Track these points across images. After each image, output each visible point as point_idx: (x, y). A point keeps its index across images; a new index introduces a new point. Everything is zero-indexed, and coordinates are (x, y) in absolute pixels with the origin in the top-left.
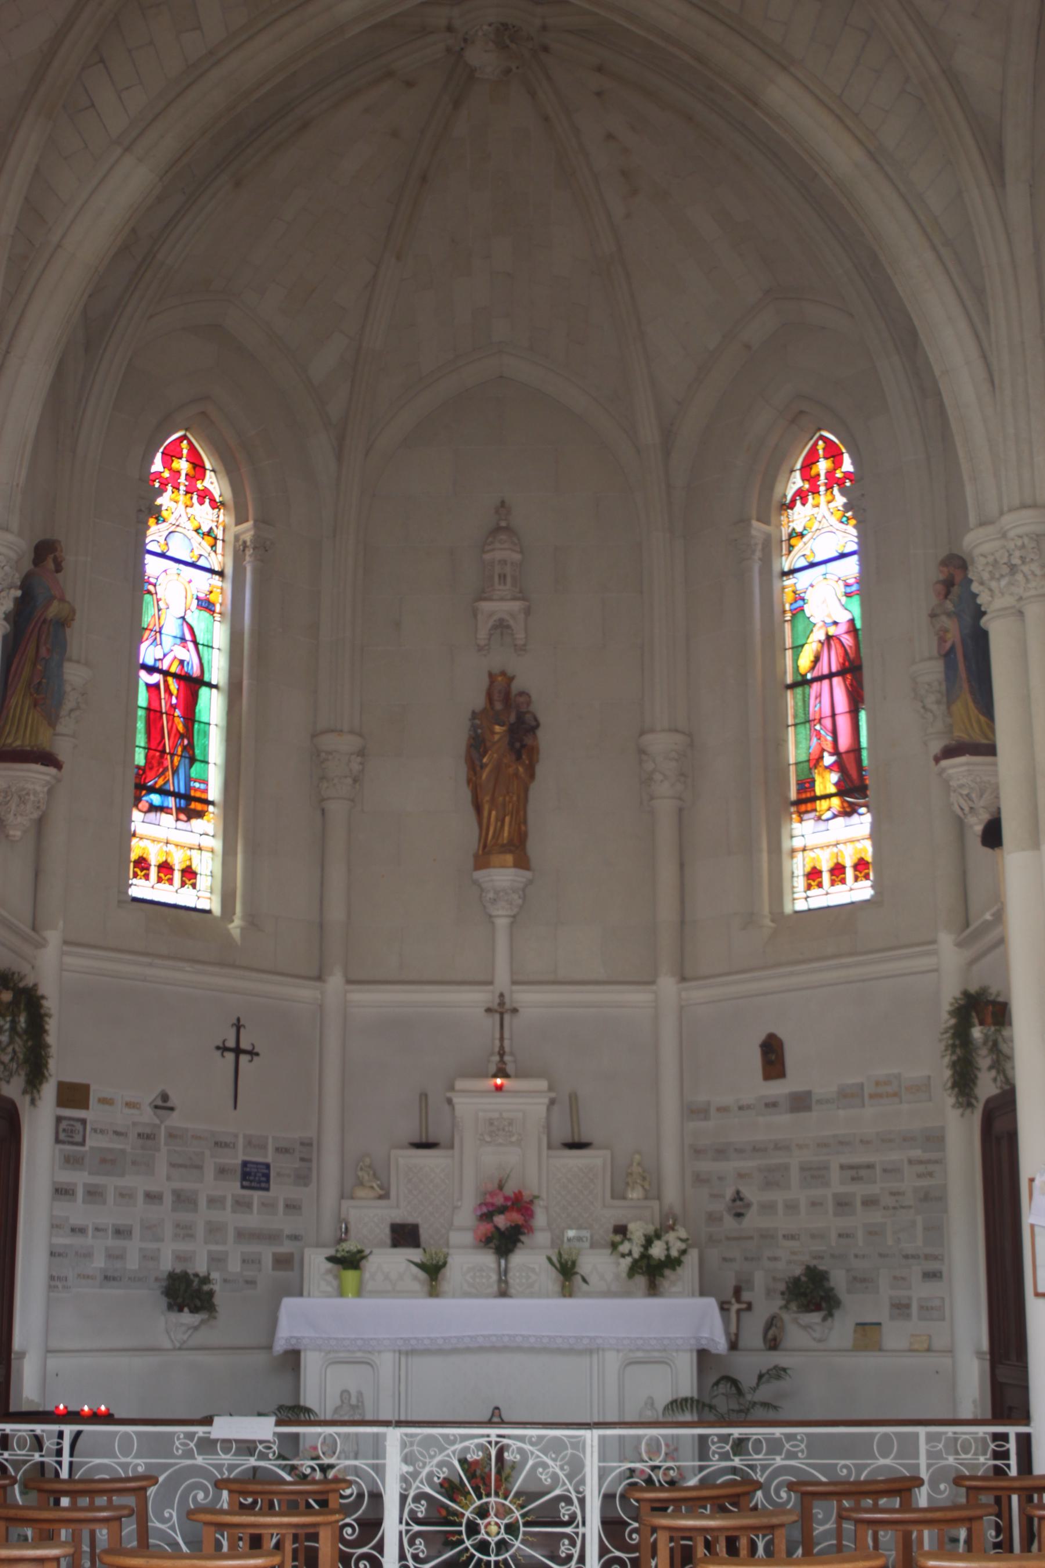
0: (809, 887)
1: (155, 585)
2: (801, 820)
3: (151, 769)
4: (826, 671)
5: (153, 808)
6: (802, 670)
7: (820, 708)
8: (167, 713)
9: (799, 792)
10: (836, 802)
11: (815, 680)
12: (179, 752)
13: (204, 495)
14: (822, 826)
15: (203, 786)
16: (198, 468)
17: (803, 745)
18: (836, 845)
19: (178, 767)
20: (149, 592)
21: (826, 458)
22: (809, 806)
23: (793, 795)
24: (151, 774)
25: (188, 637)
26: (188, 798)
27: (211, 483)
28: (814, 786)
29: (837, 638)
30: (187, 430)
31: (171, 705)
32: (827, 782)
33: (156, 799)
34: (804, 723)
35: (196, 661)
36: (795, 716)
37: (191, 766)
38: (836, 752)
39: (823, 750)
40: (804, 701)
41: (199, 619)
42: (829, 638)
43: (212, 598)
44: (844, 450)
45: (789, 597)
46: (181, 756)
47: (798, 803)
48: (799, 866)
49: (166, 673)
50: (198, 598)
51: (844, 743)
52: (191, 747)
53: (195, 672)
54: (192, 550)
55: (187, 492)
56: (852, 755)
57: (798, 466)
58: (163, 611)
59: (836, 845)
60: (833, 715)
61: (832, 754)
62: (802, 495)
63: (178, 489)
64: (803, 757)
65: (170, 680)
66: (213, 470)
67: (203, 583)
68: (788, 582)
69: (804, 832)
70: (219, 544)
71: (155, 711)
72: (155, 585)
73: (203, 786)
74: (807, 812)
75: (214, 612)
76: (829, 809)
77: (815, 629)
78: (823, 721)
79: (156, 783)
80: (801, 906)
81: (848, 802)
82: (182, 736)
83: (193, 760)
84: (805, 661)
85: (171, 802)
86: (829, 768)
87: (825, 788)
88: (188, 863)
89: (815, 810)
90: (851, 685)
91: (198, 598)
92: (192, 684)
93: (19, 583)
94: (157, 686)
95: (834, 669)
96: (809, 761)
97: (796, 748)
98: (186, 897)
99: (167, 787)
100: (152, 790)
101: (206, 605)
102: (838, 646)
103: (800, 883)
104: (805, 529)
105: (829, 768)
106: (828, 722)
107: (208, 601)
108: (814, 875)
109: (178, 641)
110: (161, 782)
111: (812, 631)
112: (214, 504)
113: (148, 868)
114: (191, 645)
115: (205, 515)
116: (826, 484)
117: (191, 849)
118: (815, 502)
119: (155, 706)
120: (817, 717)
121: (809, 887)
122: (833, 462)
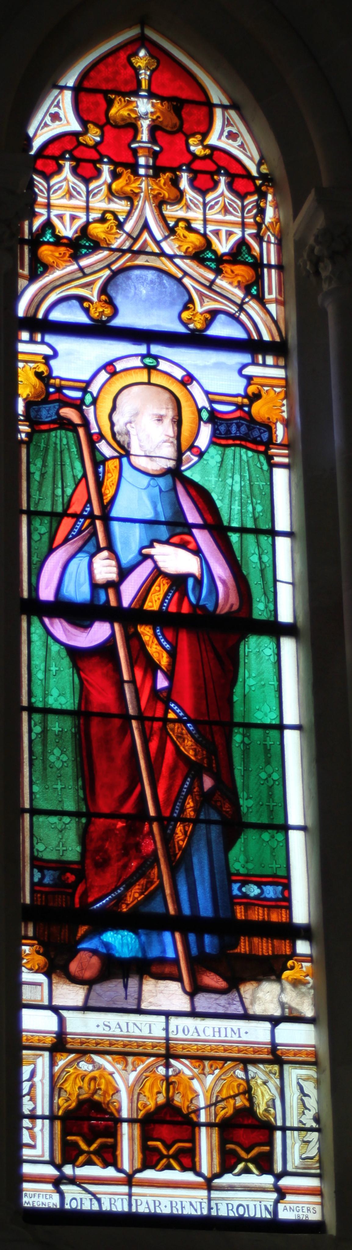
0: (69, 1154)
1: (78, 405)
3: (102, 865)
5: (114, 968)
8: (140, 718)
12: (190, 813)
13: (212, 169)
15: (270, 892)
16: (186, 111)
19: (187, 852)
20: (66, 424)
21: (151, 95)
24: (109, 876)
25: (193, 517)
26: (226, 927)
27: (229, 136)
30: (143, 24)
31: (155, 693)
33: (121, 942)
35: (220, 570)
37: (229, 844)
41: (218, 472)
43: (259, 410)
46: (195, 821)
49: (131, 617)
50: (214, 418)
52: (227, 789)
53: (225, 596)
54: (188, 304)
55: (157, 171)
57: (70, 80)
58: (112, 465)
63: (134, 167)
65: (146, 632)
66: (234, 106)
67: (219, 376)
70: (271, 278)
71: (105, 716)
72: (78, 405)
73: (270, 892)
75: (270, 442)
79: (120, 899)
82: (195, 770)
83: (233, 827)
85: (170, 945)
88: (240, 1102)
91: (214, 418)
92: (215, 632)
94: (106, 650)
98: (245, 1197)
99: (156, 907)
100: (114, 920)
101: (238, 428)
107: (250, 421)
109: (163, 532)
110: (134, 895)
112: (239, 180)
113: (113, 1132)
114: (202, 538)
115: (218, 215)
117: (245, 1062)
119: (103, 699)
121: (69, 1154)
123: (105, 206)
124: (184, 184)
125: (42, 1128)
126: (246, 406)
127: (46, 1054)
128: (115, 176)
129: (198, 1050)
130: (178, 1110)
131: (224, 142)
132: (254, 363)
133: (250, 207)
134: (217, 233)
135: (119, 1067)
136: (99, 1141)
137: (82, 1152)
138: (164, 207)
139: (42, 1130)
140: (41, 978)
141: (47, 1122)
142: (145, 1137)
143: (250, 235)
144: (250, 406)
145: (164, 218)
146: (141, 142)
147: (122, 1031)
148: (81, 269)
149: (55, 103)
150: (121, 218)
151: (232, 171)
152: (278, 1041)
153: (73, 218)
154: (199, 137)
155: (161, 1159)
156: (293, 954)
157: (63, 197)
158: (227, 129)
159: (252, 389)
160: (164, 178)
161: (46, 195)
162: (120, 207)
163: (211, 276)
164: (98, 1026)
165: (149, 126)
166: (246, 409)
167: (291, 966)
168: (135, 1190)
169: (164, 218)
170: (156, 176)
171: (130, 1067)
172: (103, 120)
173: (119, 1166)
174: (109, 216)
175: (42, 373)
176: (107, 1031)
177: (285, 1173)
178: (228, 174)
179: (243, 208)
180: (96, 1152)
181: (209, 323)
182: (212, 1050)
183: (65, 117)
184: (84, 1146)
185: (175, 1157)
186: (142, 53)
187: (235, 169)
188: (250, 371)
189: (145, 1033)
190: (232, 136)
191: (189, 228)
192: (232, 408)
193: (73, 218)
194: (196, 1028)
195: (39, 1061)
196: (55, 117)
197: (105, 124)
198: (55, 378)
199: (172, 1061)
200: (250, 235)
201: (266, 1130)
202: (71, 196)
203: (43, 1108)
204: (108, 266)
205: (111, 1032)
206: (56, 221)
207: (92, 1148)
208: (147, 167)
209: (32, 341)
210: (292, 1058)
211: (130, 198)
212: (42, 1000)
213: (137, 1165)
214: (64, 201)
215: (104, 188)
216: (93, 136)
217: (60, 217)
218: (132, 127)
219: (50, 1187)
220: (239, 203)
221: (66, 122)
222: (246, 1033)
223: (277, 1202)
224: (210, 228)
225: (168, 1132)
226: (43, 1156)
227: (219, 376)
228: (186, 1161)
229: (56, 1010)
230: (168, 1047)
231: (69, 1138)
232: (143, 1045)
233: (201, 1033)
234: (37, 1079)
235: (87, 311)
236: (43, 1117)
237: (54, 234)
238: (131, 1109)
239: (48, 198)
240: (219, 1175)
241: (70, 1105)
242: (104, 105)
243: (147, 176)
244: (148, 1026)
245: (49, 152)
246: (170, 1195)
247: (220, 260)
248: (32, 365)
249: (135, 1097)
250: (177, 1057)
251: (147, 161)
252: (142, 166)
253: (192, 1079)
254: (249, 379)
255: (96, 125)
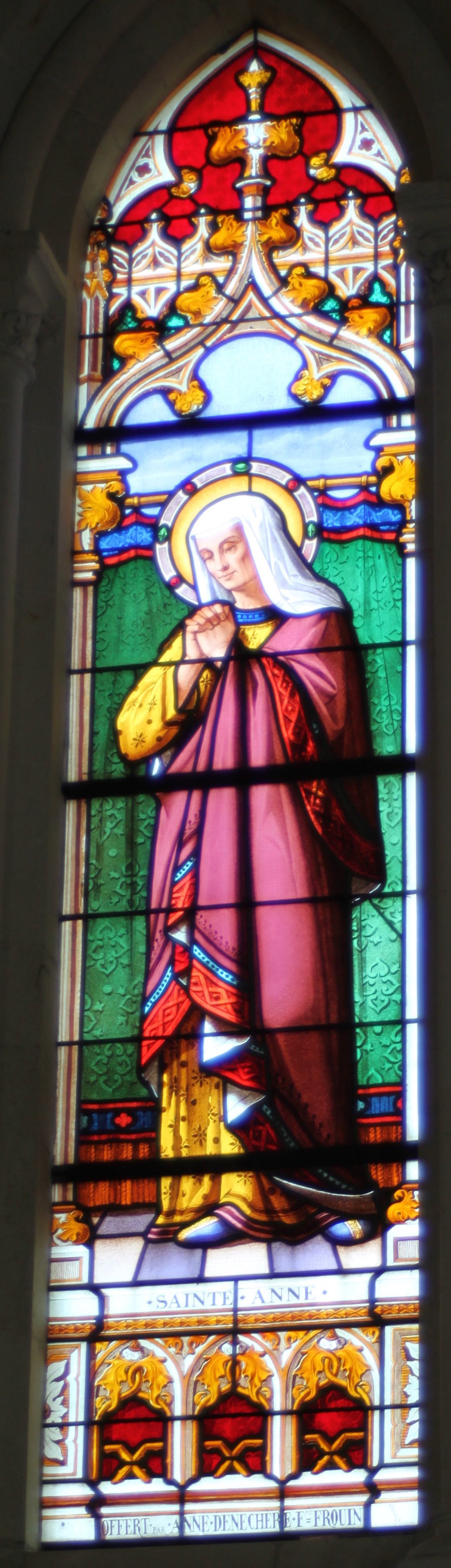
0: (107, 1468)
2: (90, 1239)
4: (225, 759)
6: (129, 745)
7: (195, 873)
9: (84, 1137)
10: (237, 1187)
11: (171, 783)
14: (177, 1263)
17: (118, 986)
18: (234, 1332)
21: (267, 115)
22: (127, 1192)
23: (63, 1147)
27: (368, 144)
28: (155, 1127)
29: (281, 663)
32: (208, 1120)
34: (129, 915)
36: (89, 888)
38: (247, 1018)
39: (196, 1014)
40: (131, 844)
42: (240, 655)
44: (345, 96)
45: (92, 507)
47: (78, 1174)
48: (69, 1388)
51: (284, 993)
55: (267, 210)
56: (314, 1043)
57: (163, 120)
59: (234, 1332)
60: (246, 905)
61: (226, 1029)
62: (171, 214)
63: (237, 213)
64: (112, 1022)
67: (339, 453)
68: (99, 465)
69: (98, 1276)
74: (115, 1209)
76: (208, 1209)
77: (192, 626)
78: (202, 918)
80: (70, 1527)
81: (288, 1194)
84: (142, 717)
86: (221, 1073)
87: (200, 1137)
89: (155, 1207)
90: (324, 816)
93: (141, 1395)
95: (258, 757)
96: (137, 1040)
97: (91, 992)
102: (279, 686)
103: (70, 1451)
104: (172, 308)
105: (221, 1073)
106: (223, 926)
108: (129, 1432)
111: (181, 627)
116: (265, 192)
118: (220, 238)
120: (181, 900)
121: (107, 1468)
122: (298, 131)
123: (200, 267)
124: (302, 219)
125: (76, 1438)
126: (372, 485)
127: (84, 1346)
128: (214, 227)
129: (399, 1310)
130: (245, 1399)
131: (356, 155)
132: (387, 428)
133: (385, 232)
134: (341, 274)
135: (172, 1350)
136: (343, 1436)
137: (123, 1463)
138: (275, 255)
139: (75, 1441)
140: (82, 1251)
141: (81, 1429)
142: (204, 1434)
143: (384, 268)
144: (378, 485)
145: (274, 268)
146: (251, 177)
147: (179, 1306)
148: (168, 354)
149: (144, 153)
150: (221, 280)
151: (365, 189)
152: (378, 1295)
153: (159, 291)
154: (324, 155)
155: (321, 1457)
156: (403, 1182)
157: (343, 248)
158: (359, 138)
159: (382, 462)
160: (275, 218)
161: (373, 244)
162: (220, 264)
163: (330, 329)
164: (150, 1303)
165: (260, 156)
166: (373, 489)
167: (399, 1197)
168: (188, 1507)
169: (274, 268)
170: (266, 216)
171: (186, 1348)
172: (200, 162)
173: (269, 1471)
174: (204, 280)
175: (117, 492)
176: (161, 1308)
177: (382, 1465)
178: (359, 194)
179: (377, 234)
180: (341, 1452)
181: (327, 389)
182: (127, 1326)
183: (156, 166)
184: (125, 1456)
185: (341, 1452)
186: (254, 66)
187: (370, 187)
188: (381, 439)
189: (208, 1306)
190: (367, 144)
191: (309, 275)
192: (354, 492)
193: (357, 271)
194: (259, 1293)
195: (74, 1356)
196: (144, 170)
197: (205, 167)
198: (133, 496)
199: (241, 1338)
200: (384, 268)
201: (358, 1412)
202: (354, 242)
203: (77, 1412)
204: (202, 343)
205: (166, 1309)
206: (137, 300)
207: (235, 1452)
208: (255, 209)
209: (91, 457)
210: (394, 1315)
211: (232, 250)
212: (79, 1279)
213: (191, 1472)
214: (150, 272)
215: (200, 246)
216: (190, 185)
217: (143, 294)
218: (239, 161)
219: (82, 1511)
220: (372, 229)
221: (156, 173)
222: (325, 1292)
223: (367, 1506)
224: (334, 268)
225: (231, 1428)
226: (74, 1474)
227: (339, 453)
228: (252, 1461)
229: (95, 1288)
230: (236, 1321)
231: (307, 1436)
232: (135, 1325)
233: (182, 1302)
234: (70, 1378)
235: (171, 404)
236: (76, 1424)
237: (135, 318)
238: (186, 1403)
239: (130, 273)
240: (295, 1476)
241: (109, 1406)
242: (204, 141)
243: (254, 219)
244: (211, 1295)
245: (132, 217)
246: (234, 1509)
247: (345, 306)
248: (103, 485)
249: (192, 1387)
250: (247, 1332)
251: (255, 201)
252: (248, 210)
253: (262, 1355)
254: (379, 450)
255: (192, 169)
